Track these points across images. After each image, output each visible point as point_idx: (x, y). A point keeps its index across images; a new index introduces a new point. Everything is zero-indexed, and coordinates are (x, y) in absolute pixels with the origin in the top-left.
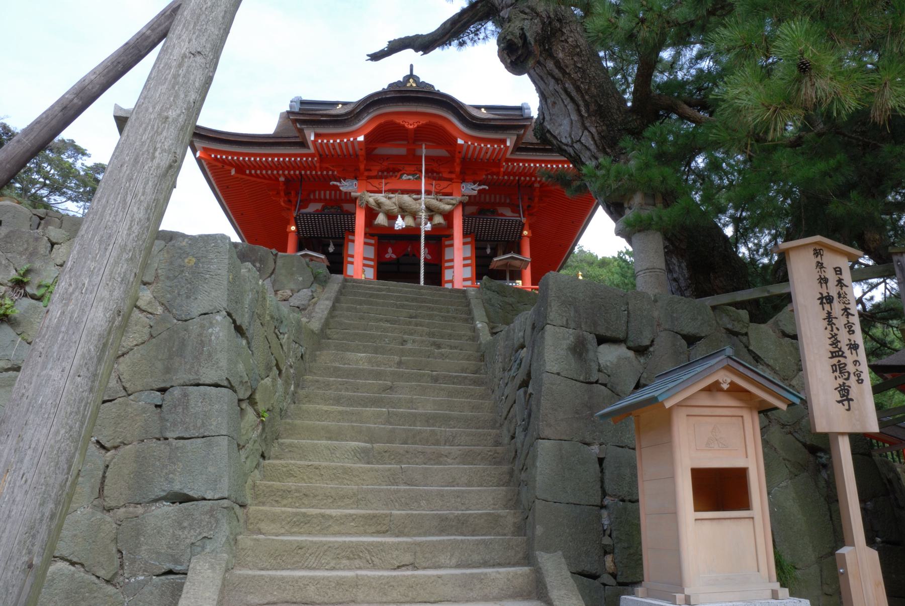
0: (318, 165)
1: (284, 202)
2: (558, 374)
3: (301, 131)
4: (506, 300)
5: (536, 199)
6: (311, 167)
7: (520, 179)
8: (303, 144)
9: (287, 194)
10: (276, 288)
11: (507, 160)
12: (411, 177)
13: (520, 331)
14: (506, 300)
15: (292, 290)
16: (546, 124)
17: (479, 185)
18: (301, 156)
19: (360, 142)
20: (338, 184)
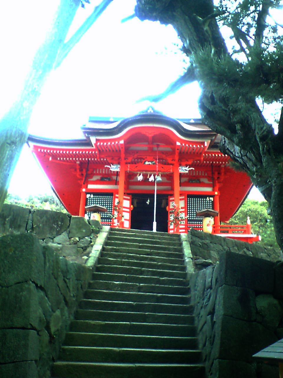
0: (98, 156)
1: (79, 175)
2: (231, 316)
3: (88, 138)
4: (204, 241)
5: (223, 174)
6: (94, 156)
7: (213, 162)
8: (89, 144)
9: (81, 170)
10: (70, 236)
11: (205, 153)
12: (150, 163)
13: (209, 278)
14: (204, 241)
15: (79, 238)
16: (226, 145)
17: (189, 168)
18: (89, 150)
19: (121, 144)
20: (109, 167)
